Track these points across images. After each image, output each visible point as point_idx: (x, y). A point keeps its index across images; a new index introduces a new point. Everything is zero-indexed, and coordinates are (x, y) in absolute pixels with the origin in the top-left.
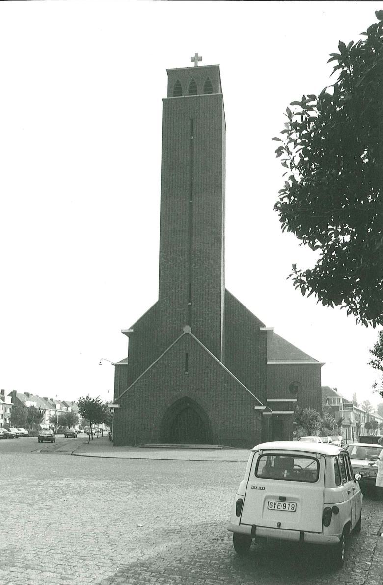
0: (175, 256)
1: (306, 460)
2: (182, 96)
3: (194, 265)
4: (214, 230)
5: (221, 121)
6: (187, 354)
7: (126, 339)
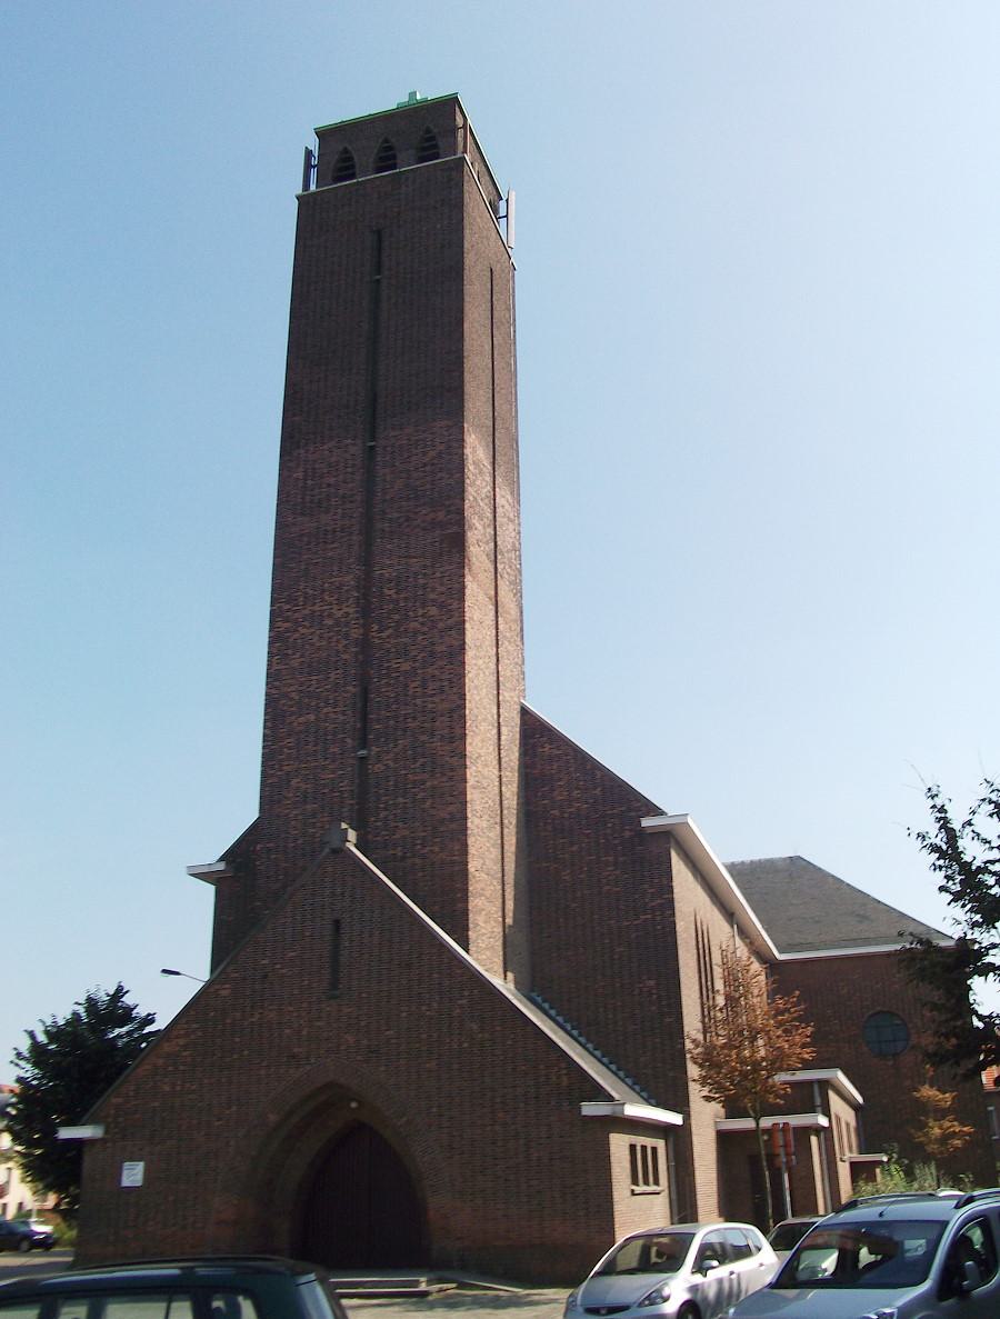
0: (316, 608)
1: (628, 1157)
2: (352, 176)
3: (376, 627)
4: (441, 516)
5: (453, 272)
6: (337, 923)
7: (209, 890)
